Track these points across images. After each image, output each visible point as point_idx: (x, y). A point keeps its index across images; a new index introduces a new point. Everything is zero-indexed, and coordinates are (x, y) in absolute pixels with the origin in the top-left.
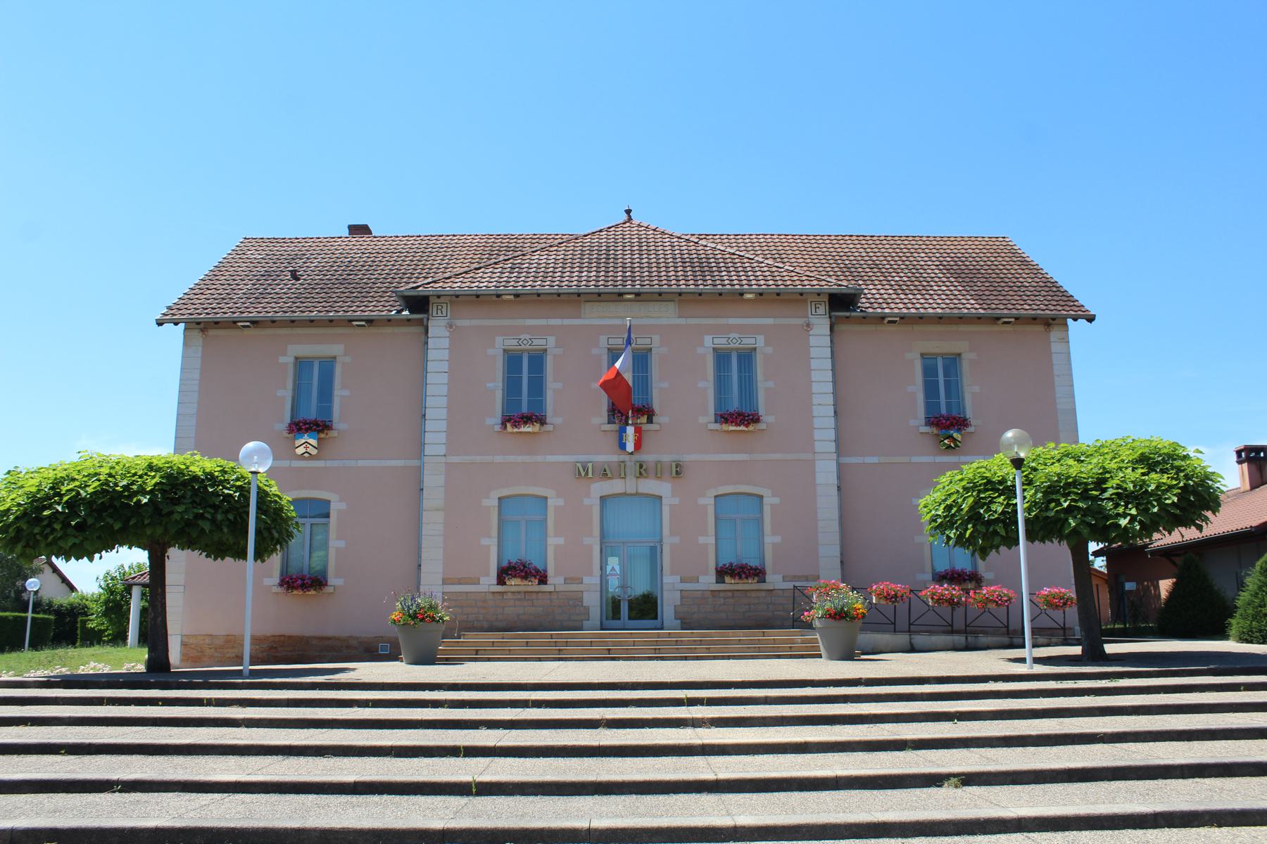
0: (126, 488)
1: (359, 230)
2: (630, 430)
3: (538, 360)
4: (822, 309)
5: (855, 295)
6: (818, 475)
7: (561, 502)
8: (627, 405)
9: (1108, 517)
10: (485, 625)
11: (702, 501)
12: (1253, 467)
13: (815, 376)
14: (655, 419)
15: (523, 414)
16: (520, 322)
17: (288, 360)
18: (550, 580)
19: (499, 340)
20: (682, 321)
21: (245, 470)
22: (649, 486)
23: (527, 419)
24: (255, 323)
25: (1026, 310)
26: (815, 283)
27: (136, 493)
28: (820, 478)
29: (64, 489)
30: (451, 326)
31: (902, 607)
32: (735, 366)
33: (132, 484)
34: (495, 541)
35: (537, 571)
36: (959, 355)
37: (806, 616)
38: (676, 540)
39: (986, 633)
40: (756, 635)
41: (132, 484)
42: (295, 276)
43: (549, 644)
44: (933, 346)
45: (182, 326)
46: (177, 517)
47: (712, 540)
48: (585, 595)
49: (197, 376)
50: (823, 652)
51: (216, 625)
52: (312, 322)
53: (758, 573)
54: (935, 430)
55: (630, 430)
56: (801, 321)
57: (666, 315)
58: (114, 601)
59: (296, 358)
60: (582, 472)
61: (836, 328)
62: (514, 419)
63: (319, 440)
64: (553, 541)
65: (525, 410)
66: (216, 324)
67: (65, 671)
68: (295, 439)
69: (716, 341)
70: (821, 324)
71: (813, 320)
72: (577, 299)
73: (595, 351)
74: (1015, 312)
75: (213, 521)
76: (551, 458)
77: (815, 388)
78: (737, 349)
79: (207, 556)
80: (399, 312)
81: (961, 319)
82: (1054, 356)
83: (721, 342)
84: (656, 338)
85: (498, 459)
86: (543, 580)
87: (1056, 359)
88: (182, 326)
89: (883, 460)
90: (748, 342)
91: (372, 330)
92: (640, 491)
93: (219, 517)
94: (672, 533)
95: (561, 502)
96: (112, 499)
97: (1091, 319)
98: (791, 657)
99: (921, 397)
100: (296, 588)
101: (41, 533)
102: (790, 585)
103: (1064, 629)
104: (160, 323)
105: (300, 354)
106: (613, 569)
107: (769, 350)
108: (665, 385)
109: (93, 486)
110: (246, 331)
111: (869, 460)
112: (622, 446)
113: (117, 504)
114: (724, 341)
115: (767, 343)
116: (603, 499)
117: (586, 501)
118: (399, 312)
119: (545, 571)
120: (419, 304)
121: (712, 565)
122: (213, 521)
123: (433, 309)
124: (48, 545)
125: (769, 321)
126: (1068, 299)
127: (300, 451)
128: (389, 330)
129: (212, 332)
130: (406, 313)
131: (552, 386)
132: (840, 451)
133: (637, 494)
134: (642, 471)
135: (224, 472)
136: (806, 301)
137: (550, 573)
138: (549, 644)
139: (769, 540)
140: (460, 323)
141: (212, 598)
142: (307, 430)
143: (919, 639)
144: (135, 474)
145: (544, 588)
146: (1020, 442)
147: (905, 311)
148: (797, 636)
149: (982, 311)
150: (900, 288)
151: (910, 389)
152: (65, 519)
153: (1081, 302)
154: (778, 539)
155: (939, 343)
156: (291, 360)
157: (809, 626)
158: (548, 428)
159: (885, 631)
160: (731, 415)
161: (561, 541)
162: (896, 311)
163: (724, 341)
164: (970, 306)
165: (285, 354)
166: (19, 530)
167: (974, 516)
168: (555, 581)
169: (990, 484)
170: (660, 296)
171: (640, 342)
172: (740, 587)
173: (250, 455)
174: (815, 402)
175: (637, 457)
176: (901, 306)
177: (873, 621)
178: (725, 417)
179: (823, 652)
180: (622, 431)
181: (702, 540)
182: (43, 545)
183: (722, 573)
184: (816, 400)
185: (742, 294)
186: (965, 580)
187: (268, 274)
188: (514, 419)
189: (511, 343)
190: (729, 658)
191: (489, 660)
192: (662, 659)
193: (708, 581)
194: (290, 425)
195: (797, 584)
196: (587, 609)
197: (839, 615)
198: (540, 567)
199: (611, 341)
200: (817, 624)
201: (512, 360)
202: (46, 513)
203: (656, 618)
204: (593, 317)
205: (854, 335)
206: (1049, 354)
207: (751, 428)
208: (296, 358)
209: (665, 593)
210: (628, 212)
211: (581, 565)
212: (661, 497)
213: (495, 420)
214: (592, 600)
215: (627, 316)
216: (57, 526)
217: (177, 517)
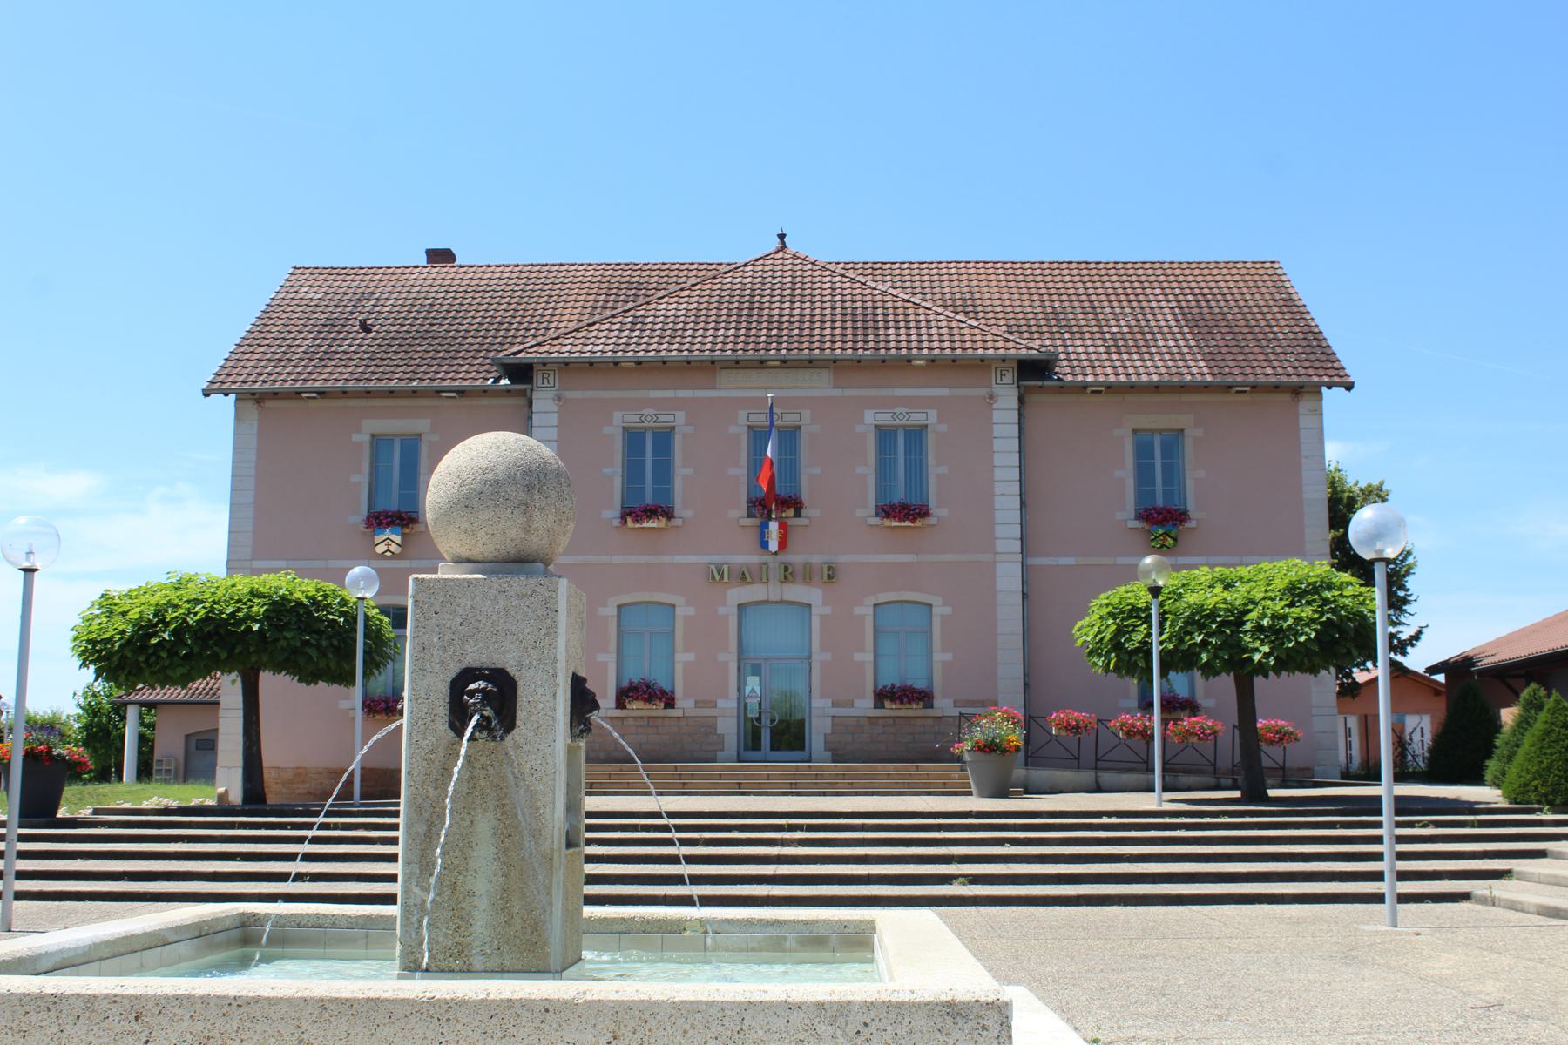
0: (232, 615)
1: (441, 256)
2: (774, 526)
3: (664, 438)
4: (1010, 377)
5: (1048, 361)
6: (999, 581)
7: (691, 611)
9: (1245, 650)
10: (602, 755)
11: (858, 611)
14: (804, 512)
15: (646, 508)
16: (641, 394)
17: (364, 438)
18: (678, 704)
19: (617, 415)
20: (837, 393)
21: (352, 594)
22: (795, 592)
23: (651, 512)
24: (322, 393)
25: (1267, 375)
26: (1000, 344)
27: (244, 620)
28: (1001, 584)
30: (559, 399)
31: (1088, 739)
32: (901, 446)
33: (239, 610)
34: (614, 656)
35: (663, 692)
37: (956, 749)
38: (828, 656)
39: (1187, 772)
41: (239, 610)
42: (365, 328)
43: (673, 777)
44: (1146, 421)
45: (232, 397)
46: (283, 643)
47: (869, 657)
48: (720, 722)
49: (254, 458)
50: (973, 789)
52: (391, 393)
53: (924, 697)
55: (774, 526)
56: (983, 392)
57: (819, 386)
58: (99, 725)
59: (373, 436)
60: (717, 576)
61: (1027, 398)
62: (636, 512)
63: (403, 535)
64: (683, 657)
65: (649, 500)
66: (275, 395)
69: (879, 417)
70: (1007, 398)
71: (998, 391)
72: (711, 367)
73: (733, 429)
75: (318, 647)
76: (679, 559)
77: (998, 474)
78: (904, 427)
79: (300, 680)
80: (497, 380)
81: (1183, 388)
82: (1303, 433)
83: (885, 418)
84: (807, 414)
85: (617, 559)
86: (670, 703)
88: (232, 397)
89: (1082, 561)
90: (917, 418)
91: (465, 402)
92: (785, 598)
93: (324, 643)
94: (823, 649)
95: (691, 611)
96: (218, 626)
97: (1349, 387)
98: (943, 794)
100: (380, 712)
101: (147, 661)
103: (1283, 768)
104: (206, 394)
105: (378, 431)
106: (753, 691)
107: (943, 428)
108: (816, 471)
109: (201, 611)
110: (312, 404)
111: (1064, 561)
112: (764, 545)
113: (222, 631)
114: (888, 416)
115: (940, 421)
116: (741, 607)
117: (721, 610)
119: (673, 692)
120: (521, 373)
121: (870, 688)
122: (318, 647)
123: (538, 379)
124: (152, 673)
125: (944, 392)
127: (380, 549)
128: (485, 401)
129: (269, 404)
132: (1025, 551)
133: (781, 602)
134: (788, 574)
135: (326, 596)
136: (989, 366)
137: (679, 694)
138: (673, 777)
139: (938, 657)
140: (570, 394)
141: (305, 722)
142: (388, 525)
143: (1106, 778)
144: (239, 601)
145: (670, 712)
146: (1159, 568)
149: (1209, 378)
150: (1116, 345)
151: (1118, 474)
152: (171, 648)
153: (1344, 363)
154: (948, 657)
155: (1155, 419)
157: (959, 759)
158: (676, 522)
159: (1065, 768)
160: (893, 507)
161: (691, 657)
162: (1101, 378)
163: (888, 416)
164: (1198, 370)
165: (359, 430)
166: (123, 657)
167: (1117, 646)
168: (684, 704)
169: (1134, 612)
170: (811, 363)
171: (787, 418)
172: (902, 713)
173: (355, 582)
174: (997, 490)
175: (783, 558)
176: (1109, 371)
177: (1033, 754)
179: (973, 789)
180: (764, 527)
181: (858, 657)
182: (147, 673)
183: (881, 696)
184: (998, 489)
185: (909, 361)
186: (1175, 708)
187: (330, 324)
188: (636, 512)
189: (633, 420)
190: (872, 794)
191: (605, 794)
192: (798, 794)
193: (865, 705)
194: (368, 518)
195: (964, 711)
196: (721, 737)
197: (989, 747)
198: (667, 688)
199: (752, 417)
200: (967, 757)
201: (633, 439)
202: (154, 641)
203: (802, 748)
204: (730, 388)
205: (1047, 408)
206: (1295, 429)
207: (918, 523)
208: (373, 436)
209: (814, 720)
210: (782, 237)
211: (715, 693)
213: (612, 513)
214: (728, 728)
215: (770, 389)
216: (164, 655)
217: (283, 643)
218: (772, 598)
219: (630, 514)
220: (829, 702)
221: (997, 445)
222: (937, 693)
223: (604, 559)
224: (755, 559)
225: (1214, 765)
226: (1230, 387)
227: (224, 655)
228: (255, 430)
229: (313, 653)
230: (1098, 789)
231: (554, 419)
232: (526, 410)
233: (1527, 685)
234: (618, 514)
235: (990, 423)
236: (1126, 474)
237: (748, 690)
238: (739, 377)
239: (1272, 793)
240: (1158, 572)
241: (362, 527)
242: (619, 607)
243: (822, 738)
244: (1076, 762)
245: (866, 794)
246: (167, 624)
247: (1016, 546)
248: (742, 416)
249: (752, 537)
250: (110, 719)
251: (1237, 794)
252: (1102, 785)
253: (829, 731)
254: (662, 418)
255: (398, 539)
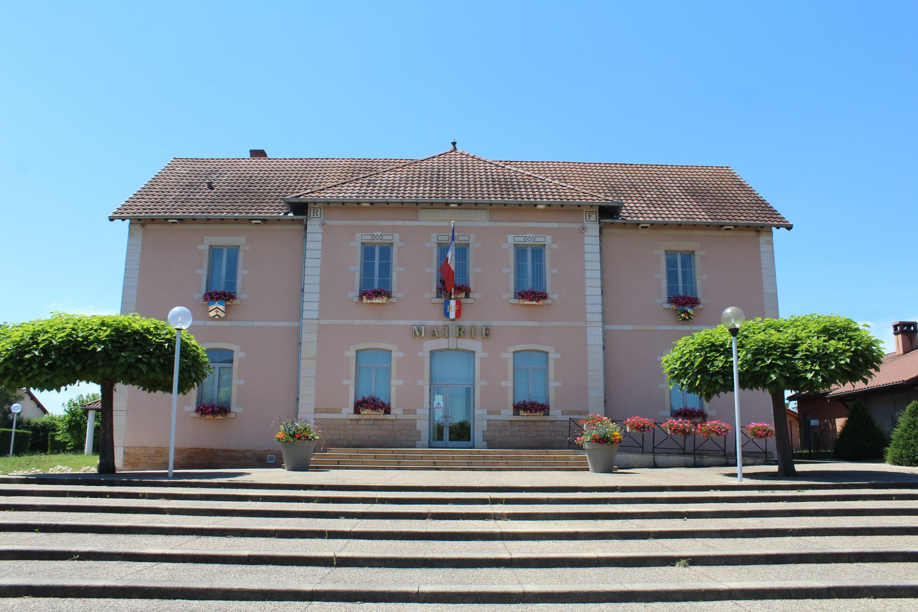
1: (258, 154)
2: (453, 303)
3: (386, 250)
4: (594, 217)
7: (401, 354)
8: (452, 285)
9: (798, 372)
11: (503, 355)
12: (906, 337)
13: (588, 266)
14: (471, 295)
15: (375, 290)
17: (204, 248)
18: (393, 411)
19: (358, 235)
20: (492, 224)
21: (172, 327)
22: (465, 343)
23: (378, 294)
24: (181, 220)
25: (742, 220)
27: (92, 343)
29: (40, 339)
30: (323, 225)
31: (648, 435)
32: (530, 257)
33: (91, 334)
34: (353, 382)
35: (383, 404)
36: (693, 252)
39: (709, 455)
40: (541, 453)
42: (210, 187)
44: (674, 246)
45: (128, 221)
46: (122, 360)
47: (511, 384)
50: (590, 466)
51: (149, 440)
52: (222, 220)
53: (544, 408)
54: (675, 307)
55: (453, 303)
56: (578, 225)
57: (480, 220)
58: (76, 420)
59: (211, 246)
60: (417, 333)
61: (604, 231)
63: (226, 306)
64: (395, 383)
65: (376, 287)
66: (153, 220)
67: (39, 471)
68: (208, 305)
69: (516, 239)
70: (593, 228)
71: (587, 225)
73: (428, 245)
74: (734, 221)
75: (148, 363)
76: (394, 322)
77: (588, 274)
78: (531, 245)
80: (286, 214)
81: (695, 226)
82: (762, 255)
83: (520, 240)
84: (473, 236)
85: (357, 322)
86: (387, 411)
87: (763, 256)
88: (128, 221)
89: (636, 327)
90: (539, 240)
91: (266, 227)
92: (459, 347)
93: (153, 361)
95: (401, 354)
96: (75, 346)
97: (789, 228)
99: (664, 282)
100: (208, 414)
101: (23, 371)
102: (566, 418)
103: (766, 453)
104: (112, 219)
106: (438, 404)
107: (555, 246)
108: (479, 270)
110: (175, 226)
111: (626, 327)
112: (447, 314)
113: (78, 350)
114: (522, 239)
115: (553, 242)
117: (420, 354)
118: (286, 214)
119: (389, 404)
120: (300, 208)
121: (511, 403)
123: (311, 213)
124: (28, 379)
125: (556, 225)
126: (773, 213)
127: (212, 314)
128: (279, 227)
129: (149, 226)
130: (291, 215)
131: (396, 270)
133: (457, 349)
134: (461, 333)
136: (582, 211)
137: (393, 405)
139: (553, 384)
140: (330, 223)
141: (147, 420)
142: (217, 299)
143: (660, 459)
145: (388, 416)
147: (654, 219)
148: (571, 455)
150: (651, 203)
152: (40, 361)
154: (559, 384)
155: (679, 243)
156: (207, 248)
157: (580, 447)
158: (393, 300)
159: (635, 452)
160: (526, 293)
161: (401, 382)
164: (702, 217)
165: (202, 243)
167: (702, 369)
168: (397, 411)
169: (713, 347)
170: (476, 206)
171: (461, 239)
172: (531, 418)
173: (175, 317)
174: (587, 284)
175: (458, 322)
176: (651, 216)
178: (522, 295)
179: (590, 466)
180: (447, 303)
181: (503, 384)
182: (24, 379)
183: (518, 408)
185: (535, 205)
186: (694, 416)
187: (191, 185)
189: (367, 238)
190: (522, 470)
191: (347, 468)
192: (473, 470)
193: (507, 413)
194: (205, 295)
195: (572, 417)
196: (420, 432)
197: (603, 440)
198: (386, 402)
199: (440, 238)
200: (586, 446)
201: (368, 251)
202: (27, 356)
203: (469, 440)
204: (427, 220)
207: (541, 303)
208: (211, 246)
210: (454, 144)
211: (416, 401)
212: (474, 352)
213: (354, 294)
214: (423, 426)
216: (35, 366)
217: (122, 360)
218: (451, 347)
219: (365, 294)
220: (486, 411)
221: (587, 257)
222: (552, 406)
223: (348, 322)
224: (441, 323)
225: (724, 451)
226: (722, 226)
227: (78, 368)
228: (140, 242)
229: (144, 368)
230: (655, 466)
231: (319, 237)
232: (303, 233)
233: (909, 402)
234: (358, 295)
235: (583, 244)
236: (662, 276)
237: (435, 403)
238: (431, 214)
239: (799, 468)
240: (736, 319)
241: (202, 301)
242: (357, 351)
243: (481, 433)
244: (641, 449)
245: (517, 470)
246: (38, 344)
247: (599, 317)
248: (434, 237)
249: (440, 310)
250: (82, 418)
251: (774, 468)
252: (658, 464)
253: (485, 429)
254: (385, 237)
255: (222, 308)
